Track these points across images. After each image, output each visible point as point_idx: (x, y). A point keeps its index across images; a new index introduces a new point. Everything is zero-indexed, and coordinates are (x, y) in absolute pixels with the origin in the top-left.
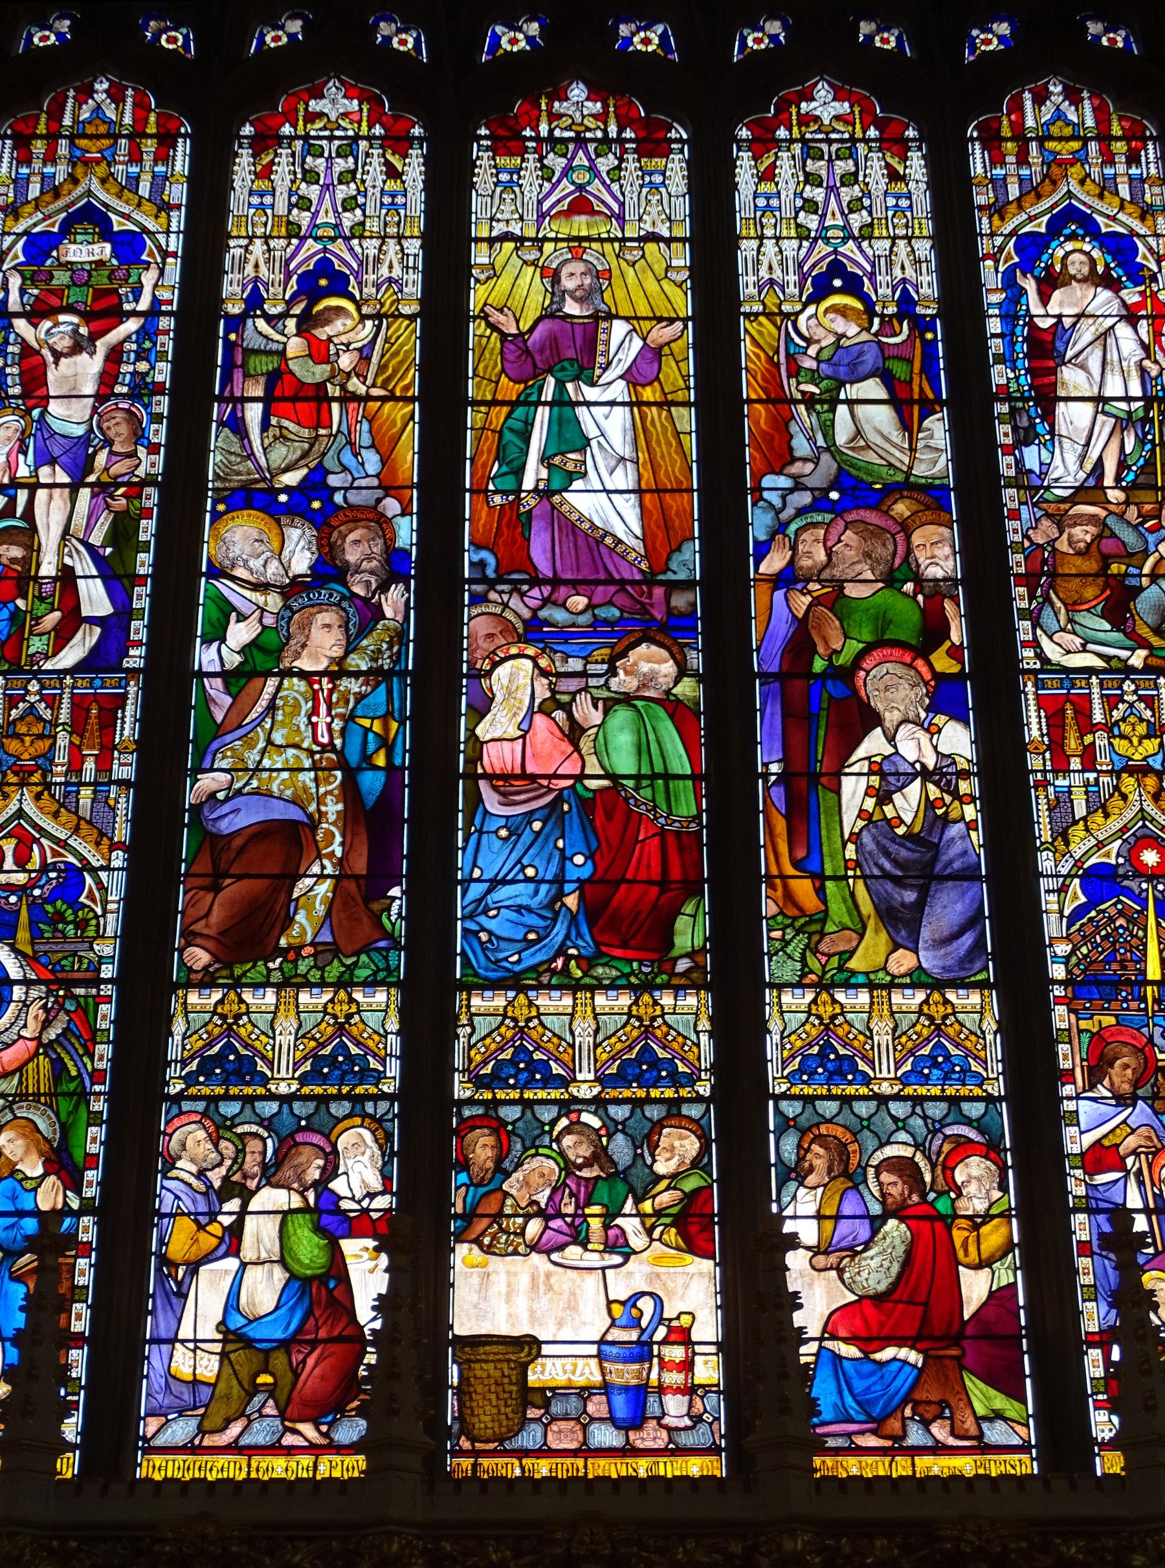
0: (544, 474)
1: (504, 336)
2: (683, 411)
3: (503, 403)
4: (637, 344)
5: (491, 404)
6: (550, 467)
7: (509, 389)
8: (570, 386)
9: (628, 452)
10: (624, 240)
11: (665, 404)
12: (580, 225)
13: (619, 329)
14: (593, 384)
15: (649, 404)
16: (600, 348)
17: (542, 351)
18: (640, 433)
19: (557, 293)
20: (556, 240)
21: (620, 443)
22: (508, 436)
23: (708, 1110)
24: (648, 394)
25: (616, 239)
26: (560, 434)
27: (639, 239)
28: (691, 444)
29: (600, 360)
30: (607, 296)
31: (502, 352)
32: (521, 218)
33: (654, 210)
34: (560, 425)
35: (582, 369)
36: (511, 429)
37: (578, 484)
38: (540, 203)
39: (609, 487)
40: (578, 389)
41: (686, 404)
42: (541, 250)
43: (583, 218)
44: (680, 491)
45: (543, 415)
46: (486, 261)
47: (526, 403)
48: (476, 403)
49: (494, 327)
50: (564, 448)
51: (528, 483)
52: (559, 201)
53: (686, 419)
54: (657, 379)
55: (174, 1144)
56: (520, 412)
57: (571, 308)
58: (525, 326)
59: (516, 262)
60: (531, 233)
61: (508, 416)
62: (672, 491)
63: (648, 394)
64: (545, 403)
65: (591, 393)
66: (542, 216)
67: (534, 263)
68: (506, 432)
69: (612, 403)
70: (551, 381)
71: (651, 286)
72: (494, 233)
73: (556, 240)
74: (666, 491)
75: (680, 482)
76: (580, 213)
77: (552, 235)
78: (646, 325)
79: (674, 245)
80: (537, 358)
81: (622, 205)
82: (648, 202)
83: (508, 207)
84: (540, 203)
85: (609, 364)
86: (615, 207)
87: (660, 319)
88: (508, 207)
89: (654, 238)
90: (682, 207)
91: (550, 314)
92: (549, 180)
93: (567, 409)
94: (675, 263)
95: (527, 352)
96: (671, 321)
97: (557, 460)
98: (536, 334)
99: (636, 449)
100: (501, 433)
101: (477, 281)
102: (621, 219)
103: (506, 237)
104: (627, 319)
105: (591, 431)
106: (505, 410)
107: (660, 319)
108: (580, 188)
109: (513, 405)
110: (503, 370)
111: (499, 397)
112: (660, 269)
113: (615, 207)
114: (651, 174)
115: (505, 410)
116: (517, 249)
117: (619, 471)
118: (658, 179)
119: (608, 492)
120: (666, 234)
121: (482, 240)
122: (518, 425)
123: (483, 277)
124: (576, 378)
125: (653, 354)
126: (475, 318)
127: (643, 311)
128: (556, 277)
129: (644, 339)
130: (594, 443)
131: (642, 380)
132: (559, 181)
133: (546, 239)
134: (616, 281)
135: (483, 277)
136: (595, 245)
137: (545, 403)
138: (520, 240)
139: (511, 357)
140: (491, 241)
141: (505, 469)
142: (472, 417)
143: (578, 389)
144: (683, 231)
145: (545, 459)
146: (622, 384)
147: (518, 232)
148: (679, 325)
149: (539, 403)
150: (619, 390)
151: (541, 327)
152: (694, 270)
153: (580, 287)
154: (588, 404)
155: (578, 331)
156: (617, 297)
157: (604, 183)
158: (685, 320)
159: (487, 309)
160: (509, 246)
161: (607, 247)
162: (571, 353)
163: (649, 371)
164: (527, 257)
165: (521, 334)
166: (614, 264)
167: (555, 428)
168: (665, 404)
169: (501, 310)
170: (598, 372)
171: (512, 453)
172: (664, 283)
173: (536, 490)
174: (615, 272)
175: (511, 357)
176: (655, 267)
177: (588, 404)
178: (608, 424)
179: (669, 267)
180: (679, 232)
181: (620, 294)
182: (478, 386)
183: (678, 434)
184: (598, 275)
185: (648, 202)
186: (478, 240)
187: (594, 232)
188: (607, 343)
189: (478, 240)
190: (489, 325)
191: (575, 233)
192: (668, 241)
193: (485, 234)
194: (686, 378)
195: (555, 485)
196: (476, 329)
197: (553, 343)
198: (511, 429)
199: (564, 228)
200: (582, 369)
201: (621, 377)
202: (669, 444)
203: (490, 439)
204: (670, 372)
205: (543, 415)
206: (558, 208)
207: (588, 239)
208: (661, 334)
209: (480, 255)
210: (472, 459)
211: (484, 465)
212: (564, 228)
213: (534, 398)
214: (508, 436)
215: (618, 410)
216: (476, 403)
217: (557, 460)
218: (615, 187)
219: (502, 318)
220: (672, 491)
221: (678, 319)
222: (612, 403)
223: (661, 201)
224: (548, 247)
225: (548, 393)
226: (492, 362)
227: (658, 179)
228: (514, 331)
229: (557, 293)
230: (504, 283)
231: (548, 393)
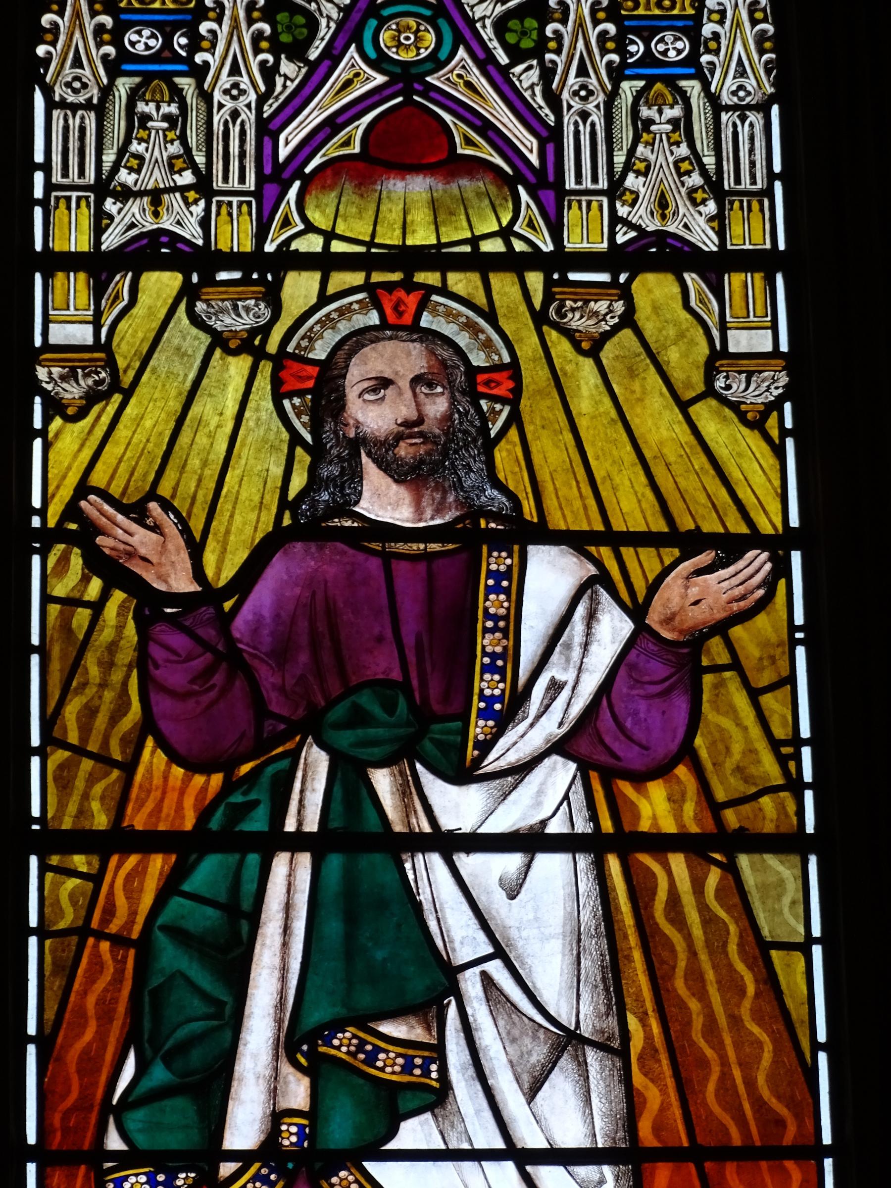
0: (298, 1092)
1: (149, 603)
2: (780, 867)
3: (148, 842)
4: (613, 628)
5: (118, 840)
6: (317, 1069)
7: (169, 790)
8: (383, 781)
9: (587, 1014)
10: (560, 262)
11: (716, 844)
12: (407, 208)
13: (550, 577)
14: (462, 773)
15: (660, 844)
16: (488, 642)
17: (281, 654)
18: (629, 944)
19: (331, 450)
20: (325, 263)
21: (555, 974)
22: (170, 957)
23: (782, 569)
24: (656, 807)
25: (535, 259)
26: (351, 949)
27: (614, 259)
28: (810, 983)
29: (488, 685)
30: (506, 457)
31: (143, 661)
32: (204, 186)
33: (662, 156)
34: (351, 918)
35: (423, 717)
36: (177, 933)
37: (415, 1132)
38: (268, 130)
39: (530, 1138)
40: (409, 790)
41: (790, 843)
42: (273, 298)
43: (418, 187)
44: (775, 1153)
45: (289, 881)
46: (83, 334)
47: (232, 841)
48: (55, 842)
49: (113, 571)
50: (365, 1000)
51: (243, 1130)
52: (332, 125)
53: (790, 896)
54: (687, 753)
55: (298, 591)
56: (208, 872)
57: (384, 501)
58: (224, 563)
59: (186, 338)
60: (236, 234)
61: (170, 887)
62: (747, 1154)
63: (656, 807)
64: (297, 842)
65: (459, 806)
66: (274, 177)
67: (250, 344)
68: (161, 939)
69: (531, 842)
70: (317, 763)
71: (659, 424)
72: (111, 240)
73: (325, 263)
74: (725, 1153)
75: (771, 1122)
76: (406, 168)
77: (313, 244)
78: (644, 563)
79: (734, 281)
80: (267, 677)
81: (550, 137)
82: (642, 127)
83: (156, 149)
84: (268, 130)
85: (518, 698)
86: (528, 144)
87: (690, 542)
88: (156, 149)
89: (666, 253)
90: (759, 146)
91: (313, 520)
92: (297, 52)
93: (375, 863)
94: (741, 341)
95: (231, 658)
96: (730, 548)
97: (342, 1045)
98: (263, 595)
99: (617, 999)
100: (144, 947)
101: (54, 407)
102: (547, 187)
103: (150, 251)
104: (577, 542)
105: (463, 940)
106: (158, 864)
107: (690, 542)
108: (406, 78)
109: (185, 847)
110: (148, 725)
111: (138, 821)
112: (686, 360)
113: (528, 144)
114: (648, 33)
115: (158, 864)
116: (188, 294)
117: (561, 1087)
118: (673, 47)
119: (524, 1158)
120: (704, 237)
121: (71, 262)
122: (203, 919)
123: (72, 392)
124: (401, 755)
125: (668, 667)
126: (48, 538)
127: (633, 510)
128: (324, 391)
129: (636, 611)
130: (471, 984)
131: (631, 757)
132: (332, 56)
133: (291, 260)
134: (539, 408)
135: (72, 392)
136: (461, 282)
137: (297, 842)
138: (198, 263)
139: (175, 677)
140: (99, 267)
141: (159, 1074)
142: (37, 888)
143: (409, 790)
144: (761, 229)
145: (298, 1042)
146: (560, 774)
147: (192, 232)
148: (756, 563)
149: (277, 841)
150: (550, 794)
151: (277, 570)
152: (798, 361)
153: (410, 427)
154: (451, 844)
155: (409, 584)
156: (539, 460)
157: (486, 62)
158: (778, 546)
159: (91, 506)
160: (160, 285)
161: (504, 286)
162: (383, 663)
163: (659, 725)
164: (226, 322)
165: (209, 595)
166: (528, 346)
167: (333, 927)
168: (716, 844)
169: (137, 512)
170: (478, 729)
171: (187, 1018)
172: (703, 412)
173: (269, 1149)
174: (534, 375)
175: (175, 677)
176: (672, 356)
177: (451, 844)
178: (523, 917)
179: (718, 358)
180: (749, 233)
181: (552, 451)
182: (63, 780)
183: (761, 949)
184: (469, 384)
185: (642, 127)
186: (57, 262)
187: (455, 232)
188: (511, 625)
189: (57, 262)
190: (99, 564)
191: (390, 237)
192: (716, 266)
193: (78, 241)
194: (785, 749)
195: (339, 1132)
196: (53, 578)
197: (317, 622)
198: (177, 933)
199: (351, 220)
200: (423, 717)
201: (560, 747)
202: (732, 986)
203: (106, 974)
204: (731, 726)
205: (289, 881)
206: (331, 150)
207: (438, 258)
208: (697, 593)
209: (64, 318)
210: (44, 1042)
211: (89, 1062)
212: (351, 220)
213: (257, 822)
214: (170, 957)
215: (552, 867)
216: (55, 842)
217: (342, 1045)
218: (527, 77)
219: (142, 539)
220: (747, 1154)
221: (755, 539)
222: (531, 842)
223: (683, 126)
224: (300, 288)
225: (309, 801)
226: (112, 696)
227: (673, 47)
228: (182, 582)
229: (331, 450)
230: (148, 414)
231: (309, 801)
